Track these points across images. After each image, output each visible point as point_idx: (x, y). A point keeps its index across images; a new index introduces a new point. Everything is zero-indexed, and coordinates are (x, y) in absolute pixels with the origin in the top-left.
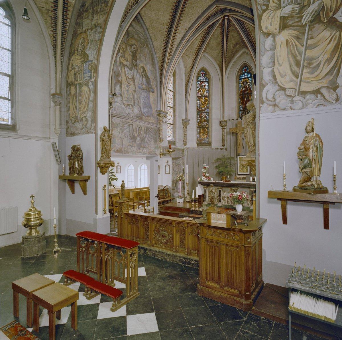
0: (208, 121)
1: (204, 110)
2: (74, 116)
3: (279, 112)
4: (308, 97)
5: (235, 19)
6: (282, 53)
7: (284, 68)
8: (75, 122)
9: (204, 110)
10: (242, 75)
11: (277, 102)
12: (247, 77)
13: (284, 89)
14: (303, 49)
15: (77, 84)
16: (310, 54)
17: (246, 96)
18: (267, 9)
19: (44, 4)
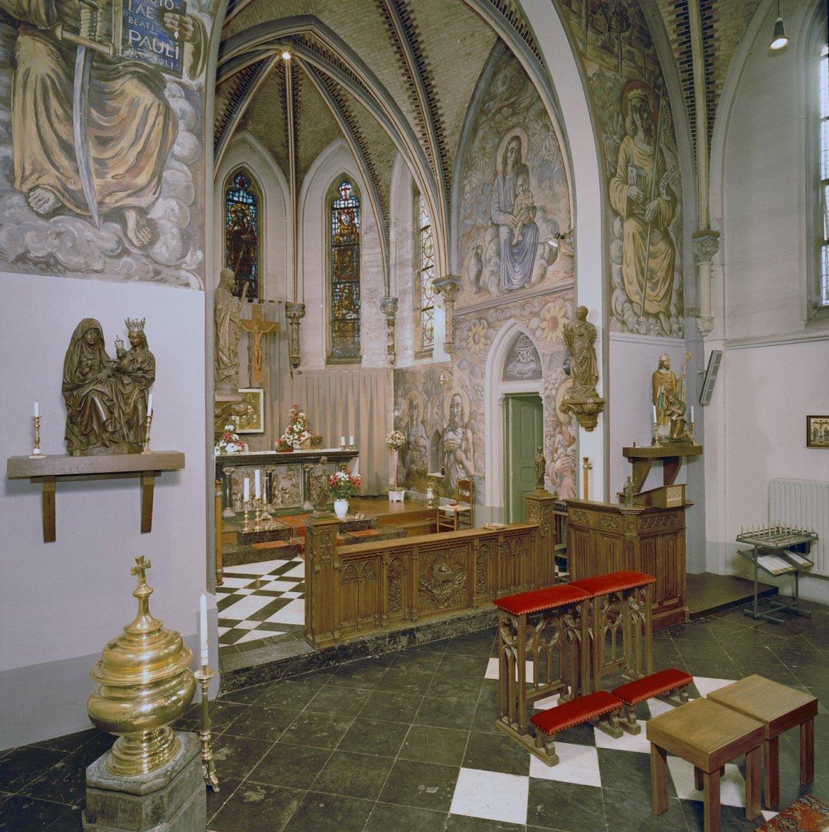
2: (50, 178)
5: (313, 70)
10: (234, 192)
11: (625, 317)
12: (245, 201)
13: (631, 302)
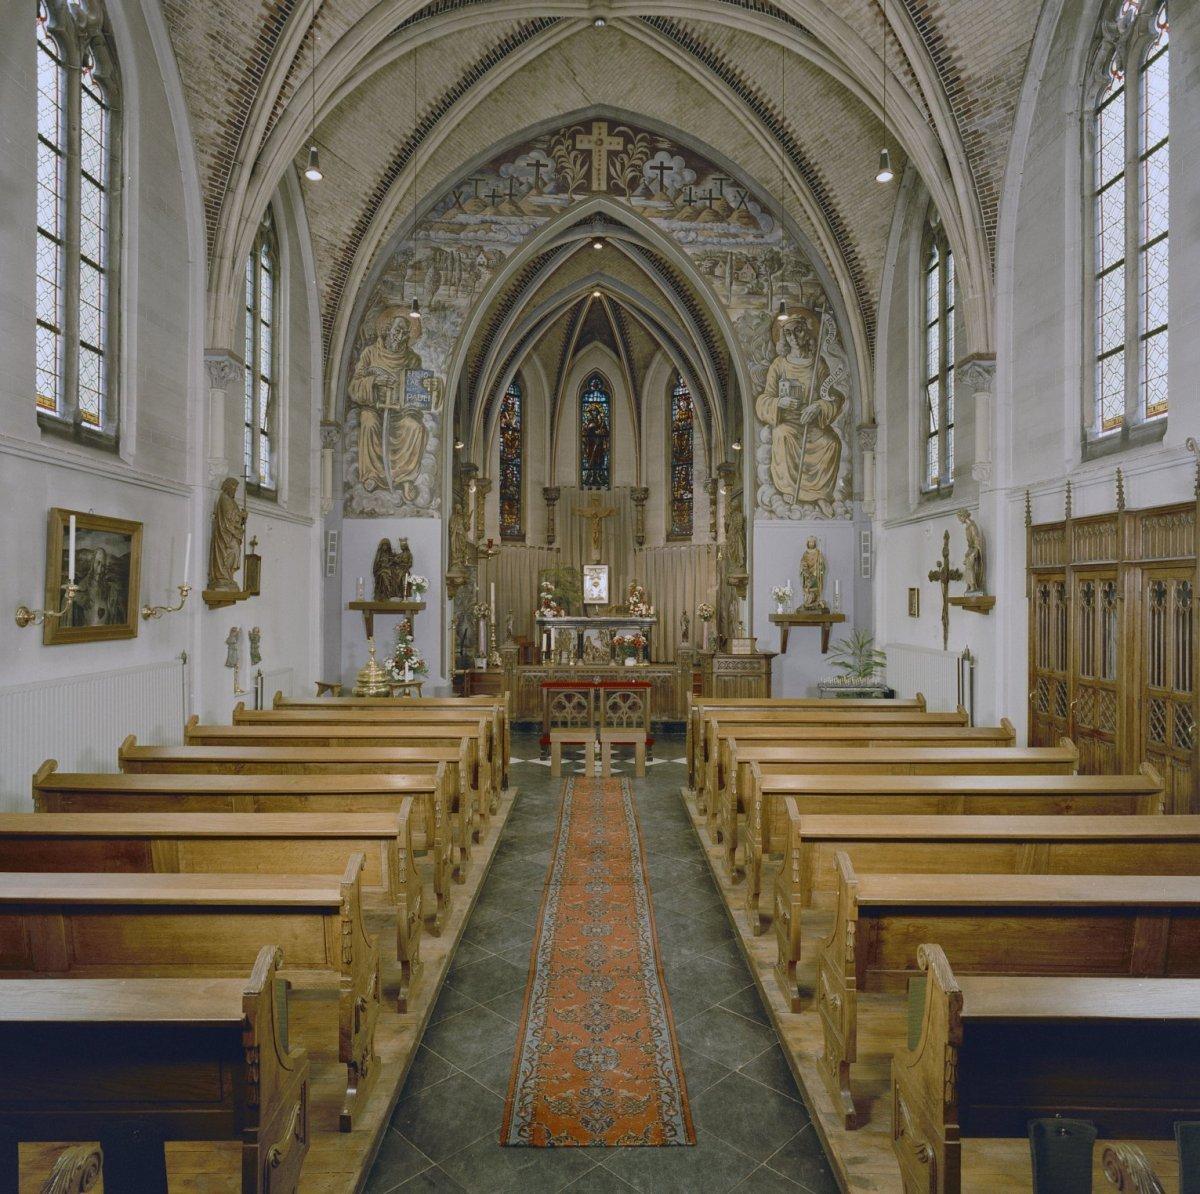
0: (518, 486)
1: (512, 460)
3: (775, 521)
4: (806, 507)
6: (779, 450)
7: (781, 469)
8: (375, 489)
9: (512, 460)
13: (781, 494)
14: (801, 452)
15: (383, 410)
16: (808, 459)
17: (597, 441)
18: (762, 392)
19: (328, 234)
